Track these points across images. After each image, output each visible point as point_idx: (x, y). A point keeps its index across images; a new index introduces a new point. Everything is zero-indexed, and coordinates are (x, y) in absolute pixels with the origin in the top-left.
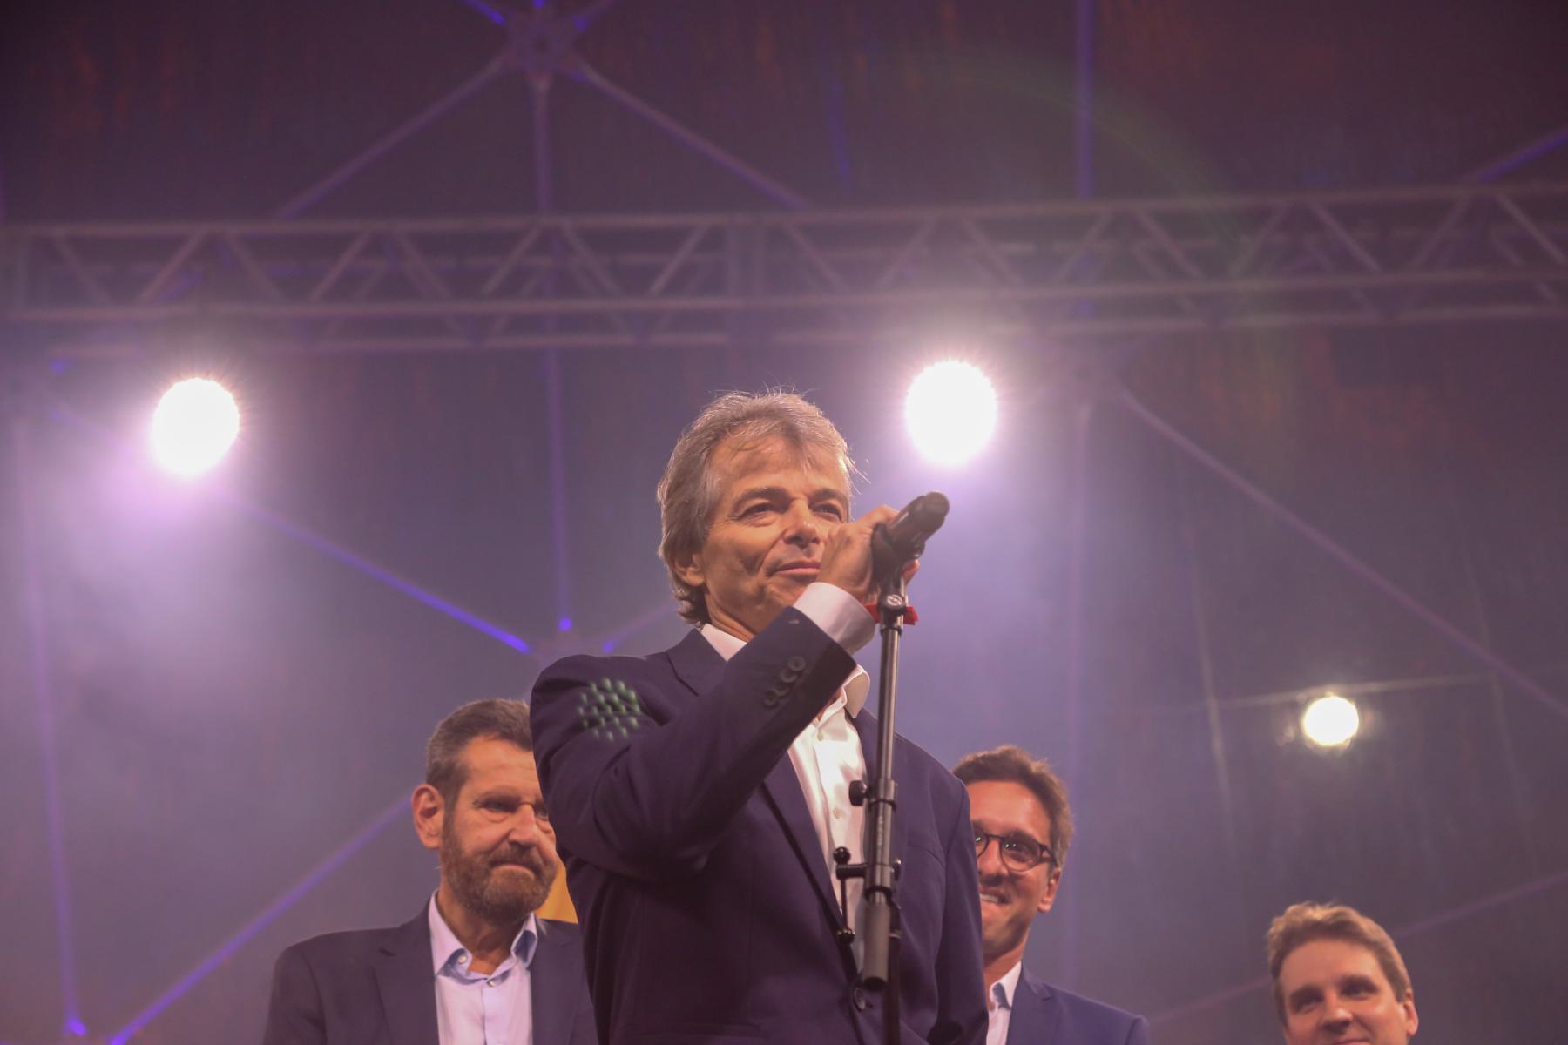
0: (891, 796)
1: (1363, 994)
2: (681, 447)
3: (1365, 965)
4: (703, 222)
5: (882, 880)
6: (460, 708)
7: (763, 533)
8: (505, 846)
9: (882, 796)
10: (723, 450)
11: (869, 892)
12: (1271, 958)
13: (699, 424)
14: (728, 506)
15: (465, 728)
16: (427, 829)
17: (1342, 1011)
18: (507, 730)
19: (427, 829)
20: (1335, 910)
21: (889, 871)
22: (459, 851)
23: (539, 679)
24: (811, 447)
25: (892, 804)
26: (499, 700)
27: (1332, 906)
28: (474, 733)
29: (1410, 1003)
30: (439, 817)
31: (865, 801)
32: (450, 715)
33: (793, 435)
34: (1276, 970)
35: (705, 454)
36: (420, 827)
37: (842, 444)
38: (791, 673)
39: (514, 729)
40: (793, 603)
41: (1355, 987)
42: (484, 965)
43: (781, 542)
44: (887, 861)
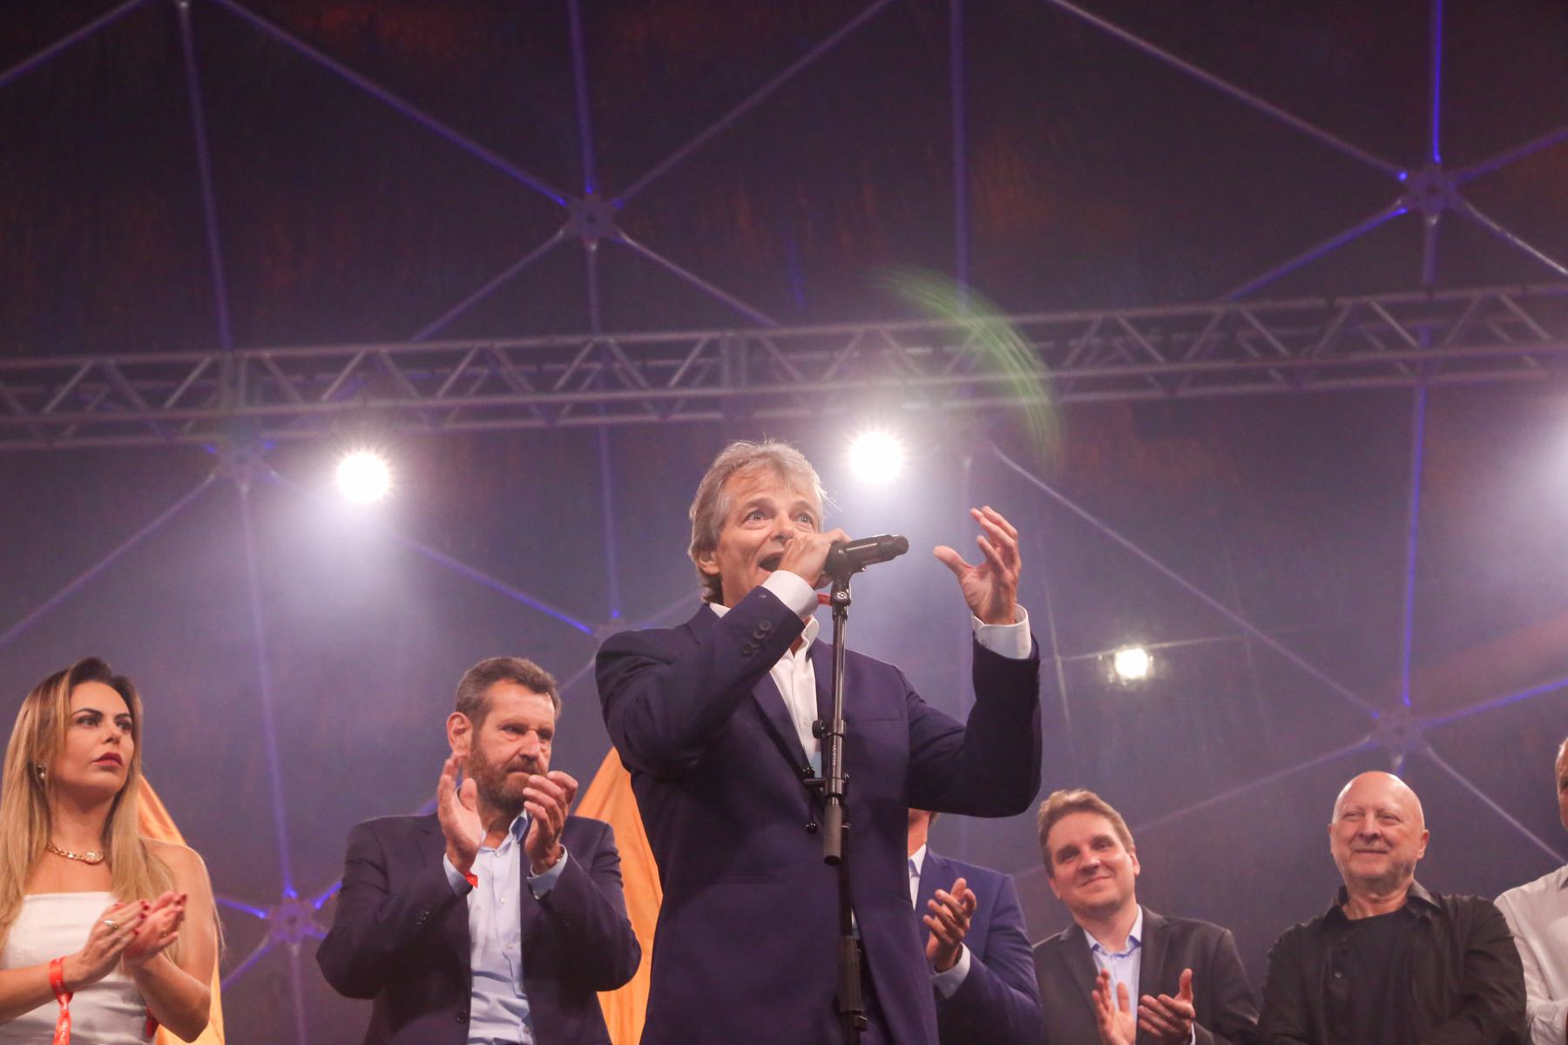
0: (841, 731)
2: (1118, 815)
3: (1105, 828)
4: (704, 336)
5: (836, 789)
6: (484, 662)
7: (755, 533)
8: (517, 759)
9: (835, 731)
10: (732, 479)
12: (1040, 831)
13: (717, 463)
14: (734, 516)
15: (488, 676)
16: (458, 743)
17: (1094, 859)
18: (522, 678)
19: (458, 743)
20: (1085, 793)
21: (840, 782)
22: (484, 761)
24: (793, 478)
25: (841, 735)
26: (514, 659)
27: (1081, 791)
28: (497, 679)
29: (1134, 855)
30: (468, 736)
32: (477, 665)
33: (780, 467)
34: (1044, 838)
35: (720, 483)
36: (453, 741)
37: (816, 477)
38: (761, 632)
39: (528, 678)
40: (762, 583)
41: (1100, 843)
42: (495, 840)
43: (769, 539)
44: (839, 776)
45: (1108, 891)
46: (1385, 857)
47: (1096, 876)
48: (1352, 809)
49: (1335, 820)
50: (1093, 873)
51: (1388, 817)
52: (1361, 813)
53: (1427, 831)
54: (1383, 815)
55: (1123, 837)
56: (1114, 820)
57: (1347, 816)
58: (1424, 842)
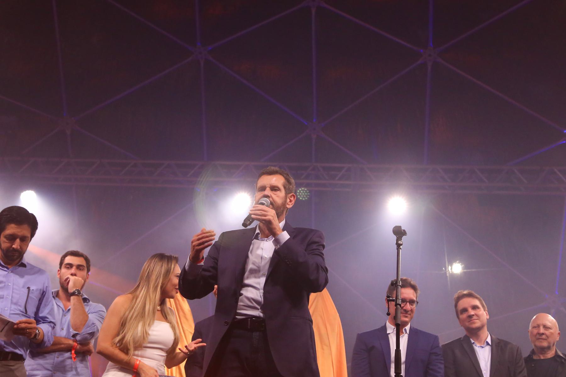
1: (477, 309)
2: (481, 299)
3: (477, 303)
11: (396, 305)
17: (472, 312)
23: (392, 325)
29: (487, 312)
31: (394, 286)
41: (475, 307)
45: (477, 324)
46: (546, 341)
47: (472, 319)
48: (535, 325)
49: (530, 328)
50: (472, 318)
51: (547, 328)
52: (538, 326)
53: (559, 332)
54: (546, 327)
55: (483, 306)
56: (480, 300)
57: (534, 327)
58: (558, 335)
